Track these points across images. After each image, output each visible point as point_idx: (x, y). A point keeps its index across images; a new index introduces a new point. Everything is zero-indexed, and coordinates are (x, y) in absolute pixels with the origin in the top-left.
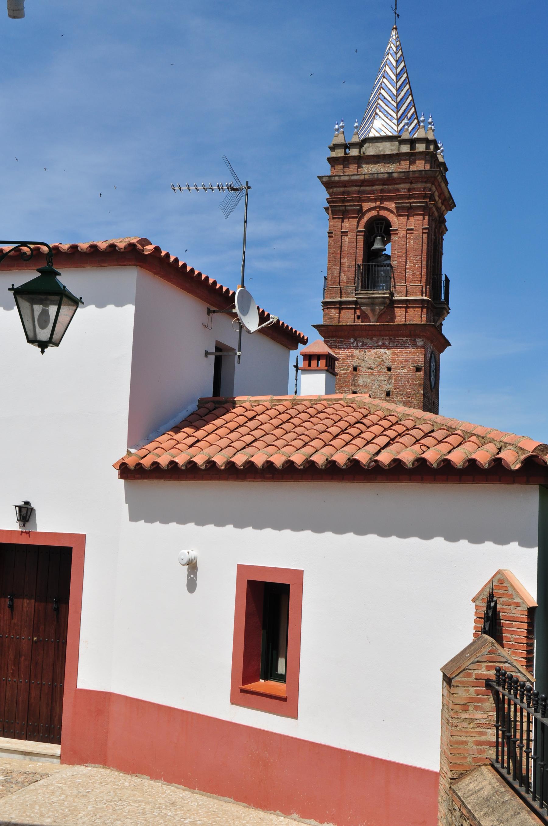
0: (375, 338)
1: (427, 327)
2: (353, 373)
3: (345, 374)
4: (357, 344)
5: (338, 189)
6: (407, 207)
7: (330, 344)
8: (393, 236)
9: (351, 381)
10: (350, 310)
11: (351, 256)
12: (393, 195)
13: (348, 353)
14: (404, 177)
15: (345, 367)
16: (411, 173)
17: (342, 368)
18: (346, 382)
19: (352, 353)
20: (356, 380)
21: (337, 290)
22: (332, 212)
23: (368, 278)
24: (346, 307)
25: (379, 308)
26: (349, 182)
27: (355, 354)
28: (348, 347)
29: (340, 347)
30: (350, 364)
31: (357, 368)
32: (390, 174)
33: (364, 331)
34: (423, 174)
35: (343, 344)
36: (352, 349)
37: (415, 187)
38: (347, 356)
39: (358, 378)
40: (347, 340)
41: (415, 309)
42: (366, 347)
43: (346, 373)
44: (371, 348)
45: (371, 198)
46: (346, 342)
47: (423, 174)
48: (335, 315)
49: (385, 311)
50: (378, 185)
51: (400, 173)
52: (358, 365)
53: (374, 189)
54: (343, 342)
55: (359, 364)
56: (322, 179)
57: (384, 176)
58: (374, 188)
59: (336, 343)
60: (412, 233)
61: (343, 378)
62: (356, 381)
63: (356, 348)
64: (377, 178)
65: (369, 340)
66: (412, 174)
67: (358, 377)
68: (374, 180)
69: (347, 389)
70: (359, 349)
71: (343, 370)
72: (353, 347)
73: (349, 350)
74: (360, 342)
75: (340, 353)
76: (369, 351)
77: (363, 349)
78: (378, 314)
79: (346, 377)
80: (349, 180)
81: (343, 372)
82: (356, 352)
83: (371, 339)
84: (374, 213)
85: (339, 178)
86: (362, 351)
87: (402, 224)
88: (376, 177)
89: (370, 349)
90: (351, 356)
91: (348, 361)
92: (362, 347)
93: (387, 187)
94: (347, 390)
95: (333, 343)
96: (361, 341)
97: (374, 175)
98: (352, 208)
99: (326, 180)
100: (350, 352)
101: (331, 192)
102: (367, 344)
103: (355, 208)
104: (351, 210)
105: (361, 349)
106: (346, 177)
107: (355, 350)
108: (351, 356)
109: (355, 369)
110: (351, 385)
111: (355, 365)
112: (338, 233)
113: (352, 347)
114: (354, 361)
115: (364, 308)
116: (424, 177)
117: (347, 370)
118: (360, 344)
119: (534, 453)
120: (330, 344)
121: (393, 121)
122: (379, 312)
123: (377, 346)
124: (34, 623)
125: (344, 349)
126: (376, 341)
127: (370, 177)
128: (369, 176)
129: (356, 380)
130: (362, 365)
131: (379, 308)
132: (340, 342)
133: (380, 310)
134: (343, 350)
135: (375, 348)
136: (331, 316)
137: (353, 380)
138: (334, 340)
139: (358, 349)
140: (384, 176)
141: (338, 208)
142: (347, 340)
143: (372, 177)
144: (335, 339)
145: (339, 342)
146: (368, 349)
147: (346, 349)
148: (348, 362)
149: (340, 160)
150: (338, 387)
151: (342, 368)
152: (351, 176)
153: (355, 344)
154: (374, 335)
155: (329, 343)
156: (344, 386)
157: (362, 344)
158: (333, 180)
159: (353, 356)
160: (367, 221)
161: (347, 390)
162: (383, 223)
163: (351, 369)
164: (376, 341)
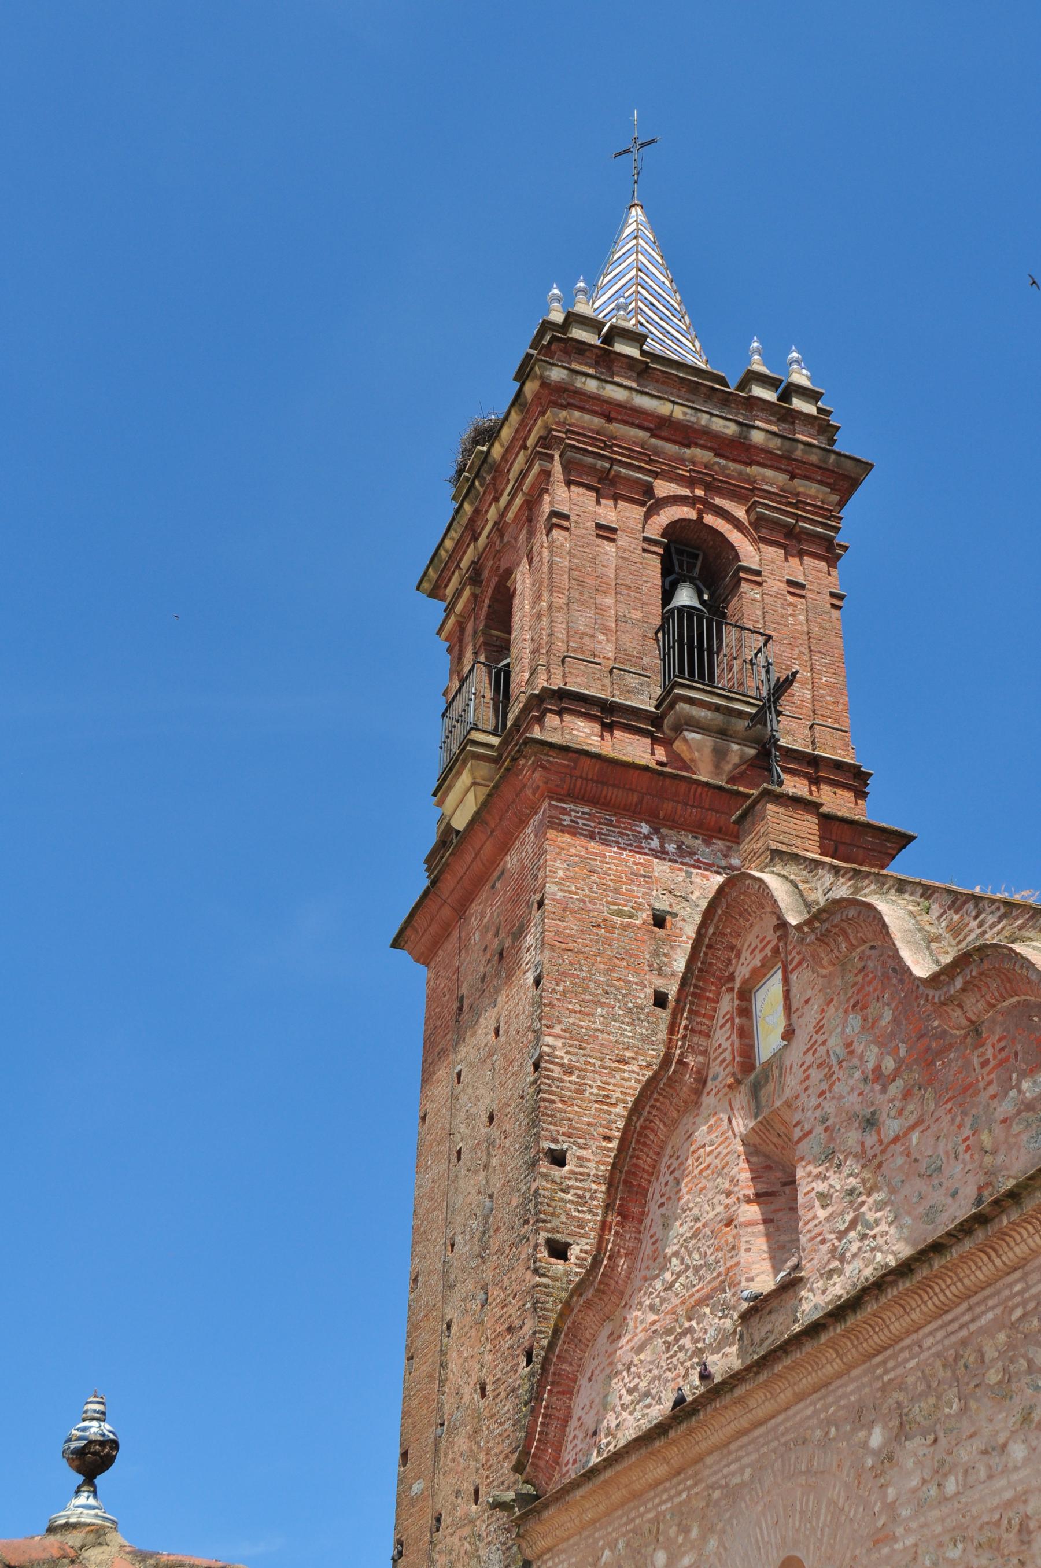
0: (720, 842)
1: (889, 845)
2: (652, 932)
3: (626, 927)
4: (662, 845)
5: (587, 417)
6: (786, 525)
7: (571, 821)
8: (745, 587)
9: (647, 956)
10: (638, 737)
11: (629, 595)
12: (743, 488)
13: (634, 863)
14: (778, 452)
15: (626, 906)
16: (801, 446)
17: (616, 907)
18: (631, 955)
19: (647, 866)
20: (665, 955)
21: (590, 670)
22: (564, 467)
23: (451, 770)
24: (627, 724)
25: (742, 751)
26: (626, 408)
27: (656, 874)
28: (631, 845)
29: (605, 840)
30: (640, 900)
31: (664, 920)
32: (745, 429)
33: (693, 806)
34: (831, 461)
35: (614, 832)
36: (645, 854)
37: (801, 489)
38: (632, 873)
39: (671, 953)
40: (629, 824)
41: (838, 791)
42: (692, 862)
43: (628, 925)
44: (708, 867)
45: (681, 472)
46: (625, 828)
47: (831, 461)
48: (588, 736)
49: (744, 772)
50: (703, 447)
51: (770, 436)
52: (668, 909)
53: (687, 456)
54: (614, 826)
55: (671, 906)
56: (551, 370)
57: (728, 427)
58: (687, 452)
59: (592, 824)
60: (803, 597)
61: (618, 940)
62: (665, 960)
63: (661, 854)
64: (706, 426)
65: (699, 842)
66: (802, 450)
67: (672, 947)
68: (696, 431)
69: (636, 980)
70: (670, 860)
71: (620, 913)
72: (650, 849)
73: (638, 856)
74: (671, 841)
75: (605, 857)
76: (703, 876)
77: (682, 863)
78: (731, 771)
79: (630, 939)
80: (627, 402)
81: (618, 920)
82: (660, 868)
83: (707, 843)
84: (688, 513)
85: (598, 388)
86: (681, 870)
87: (773, 562)
88: (703, 422)
89: (706, 870)
90: (645, 876)
91: (636, 889)
92: (680, 857)
93: (723, 462)
94: (637, 984)
95: (579, 821)
96: (675, 838)
97: (699, 414)
98: (631, 473)
99: (558, 379)
100: (640, 864)
101: (562, 420)
102: (695, 854)
103: (640, 476)
104: (628, 479)
105: (676, 862)
106: (621, 390)
107: (656, 861)
108: (645, 876)
109: (659, 920)
110: (647, 968)
111: (657, 905)
112: (588, 524)
113: (647, 851)
114: (654, 893)
115: (693, 739)
116: (832, 471)
117: (631, 917)
118: (671, 848)
119: (941, 1240)
120: (571, 821)
121: (430, 570)
122: (737, 766)
123: (724, 868)
124: (717, 416)
125: (619, 848)
126: (721, 851)
127: (688, 418)
128: (685, 414)
129: (665, 955)
130: (682, 913)
131: (742, 751)
132: (605, 824)
133: (741, 757)
134: (615, 849)
135: (721, 870)
136: (577, 736)
137: (656, 954)
138: (583, 813)
139: (665, 859)
140: (728, 427)
141: (589, 460)
142: (629, 824)
143: (693, 419)
144: (586, 810)
145: (600, 823)
146: (699, 868)
147: (625, 849)
148: (633, 891)
149: (588, 354)
150: (602, 966)
151: (616, 907)
152: (634, 393)
153: (655, 843)
154: (720, 830)
155: (565, 817)
156: (625, 968)
157: (679, 848)
158: (578, 385)
159: (649, 877)
160: (668, 525)
161: (637, 984)
162: (698, 555)
163: (644, 916)
164: (721, 851)
